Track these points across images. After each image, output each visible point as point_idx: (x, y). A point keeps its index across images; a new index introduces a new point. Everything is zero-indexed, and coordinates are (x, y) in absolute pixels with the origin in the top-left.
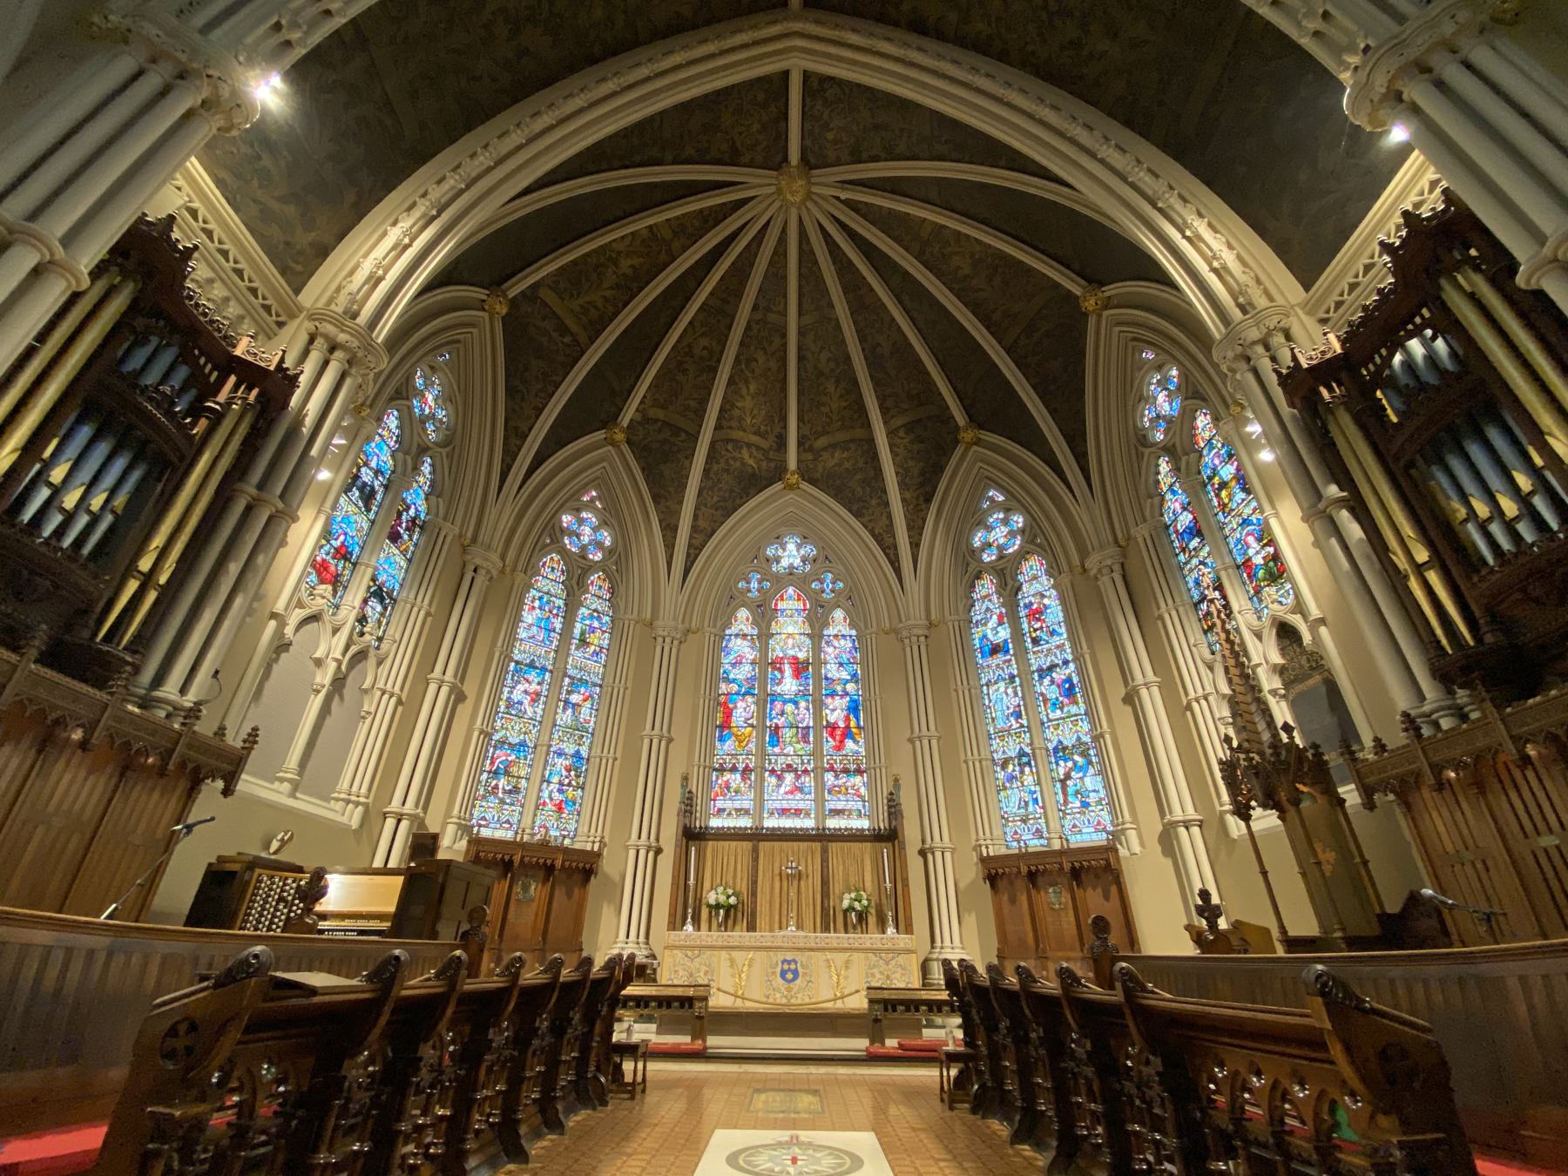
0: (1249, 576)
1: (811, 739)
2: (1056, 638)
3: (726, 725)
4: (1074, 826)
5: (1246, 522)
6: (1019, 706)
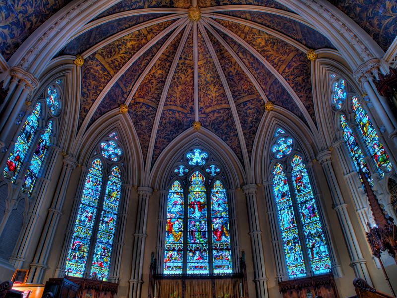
0: (376, 161)
1: (207, 236)
2: (307, 189)
4: (317, 267)
6: (293, 218)
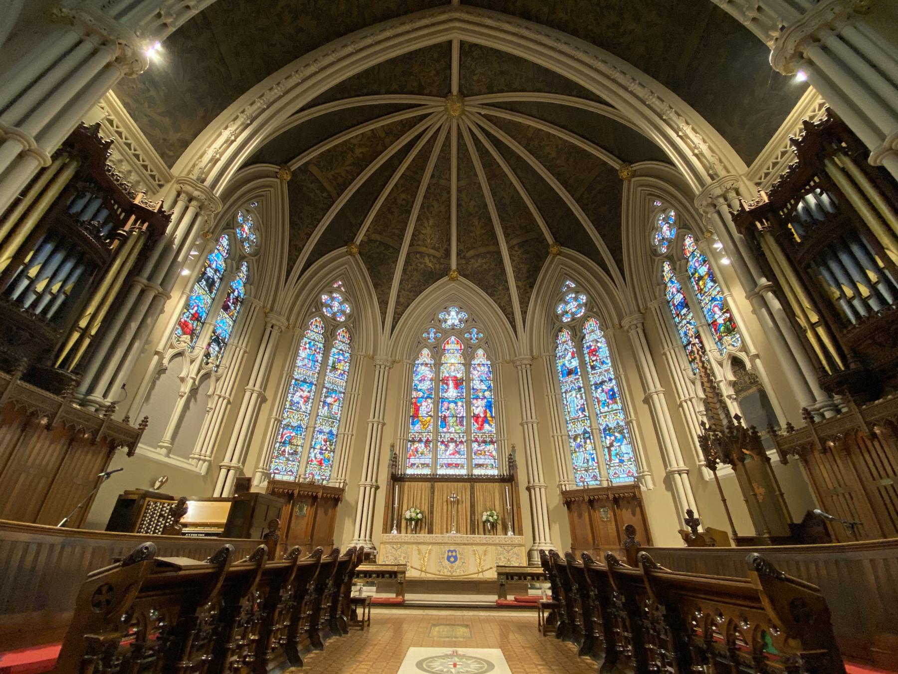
0: (715, 330)
1: (465, 423)
2: (605, 366)
3: (416, 415)
4: (615, 473)
5: (713, 299)
6: (584, 404)
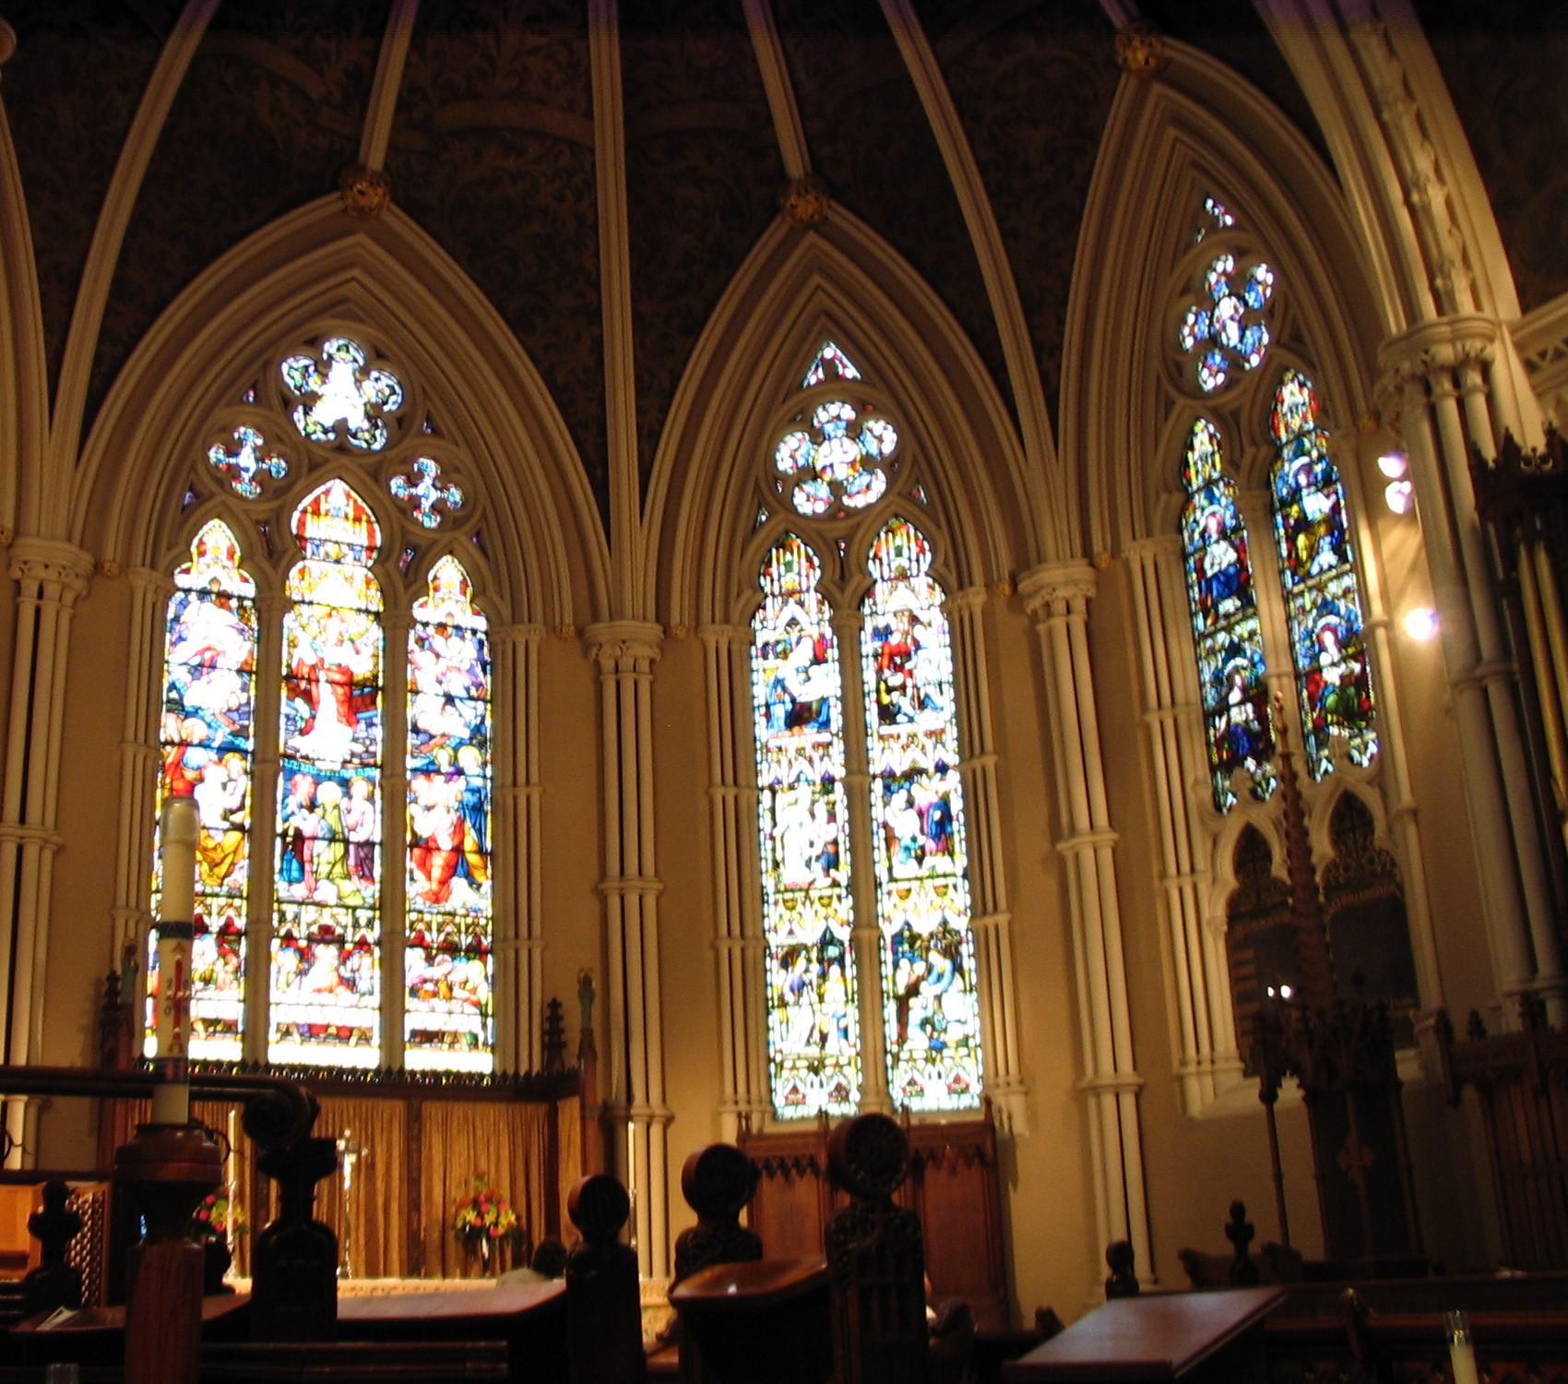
4: (912, 1082)
5: (1326, 607)
6: (835, 842)
